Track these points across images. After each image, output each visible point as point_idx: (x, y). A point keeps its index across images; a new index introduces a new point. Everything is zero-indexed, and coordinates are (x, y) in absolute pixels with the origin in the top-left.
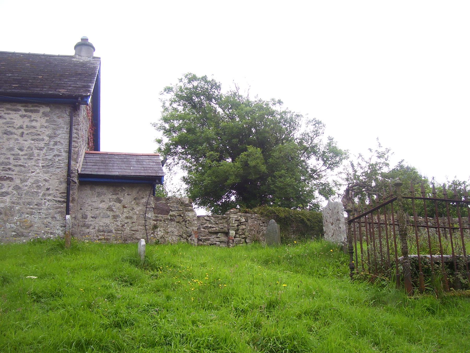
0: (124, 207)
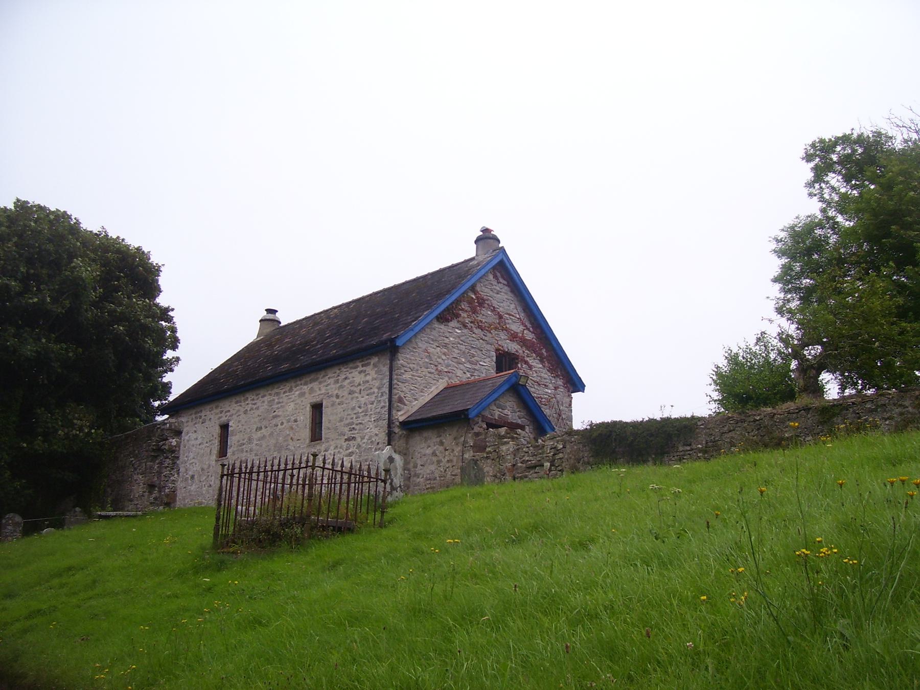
0: (446, 450)
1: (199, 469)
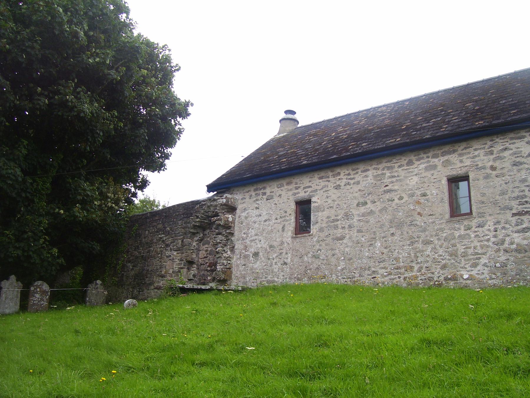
1: (265, 246)
